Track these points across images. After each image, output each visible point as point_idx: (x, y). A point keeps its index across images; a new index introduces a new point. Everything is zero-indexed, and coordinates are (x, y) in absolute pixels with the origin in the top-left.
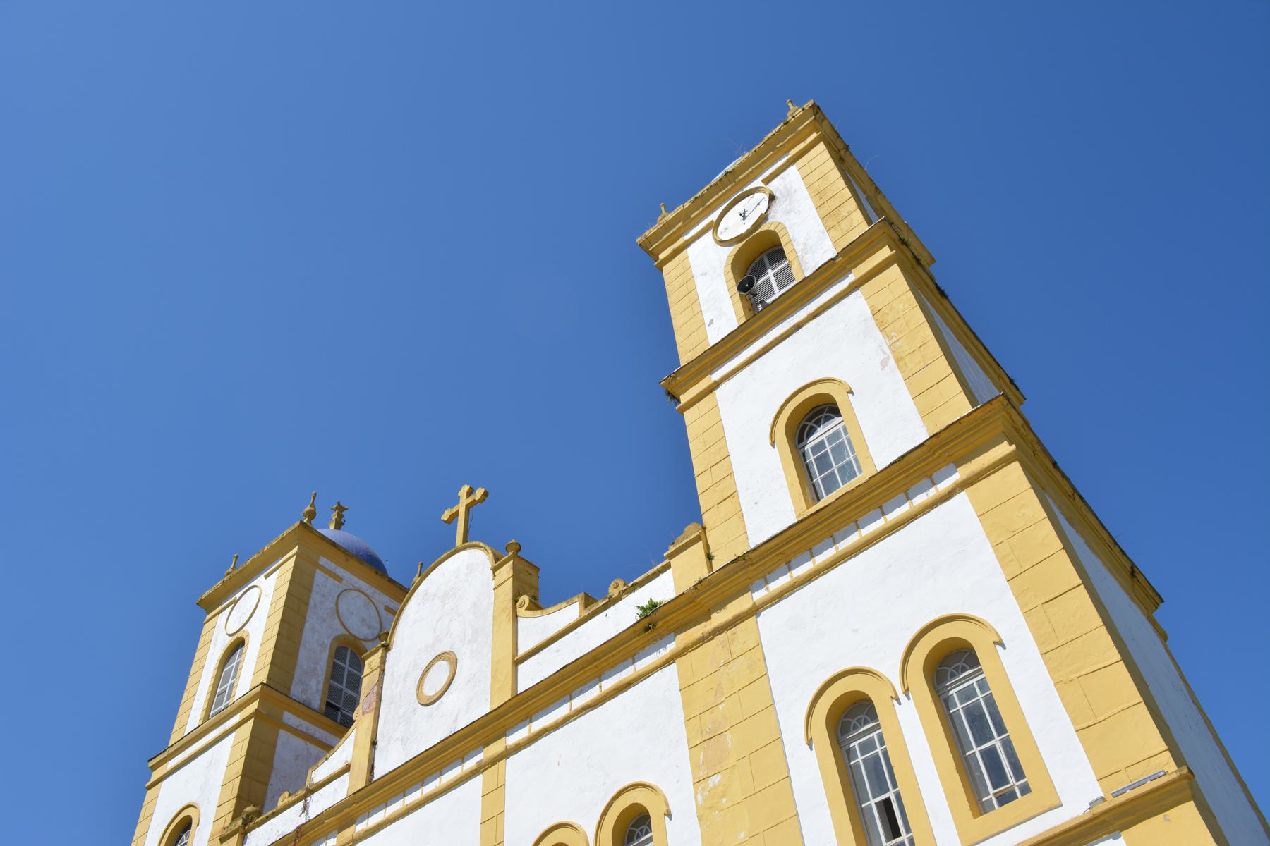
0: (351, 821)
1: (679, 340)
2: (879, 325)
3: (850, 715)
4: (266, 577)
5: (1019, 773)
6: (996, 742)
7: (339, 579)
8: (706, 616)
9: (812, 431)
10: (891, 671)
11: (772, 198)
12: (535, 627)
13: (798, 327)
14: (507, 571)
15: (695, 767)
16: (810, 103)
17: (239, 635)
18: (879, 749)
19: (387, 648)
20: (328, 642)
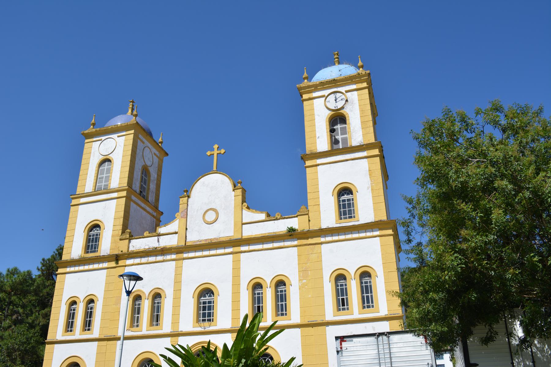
0: (182, 252)
1: (307, 137)
2: (370, 175)
4: (118, 137)
5: (372, 302)
6: (370, 295)
7: (143, 143)
8: (307, 238)
9: (343, 195)
11: (347, 101)
12: (249, 215)
13: (347, 160)
14: (239, 192)
15: (299, 276)
16: (368, 72)
17: (108, 157)
19: (189, 197)
20: (141, 168)
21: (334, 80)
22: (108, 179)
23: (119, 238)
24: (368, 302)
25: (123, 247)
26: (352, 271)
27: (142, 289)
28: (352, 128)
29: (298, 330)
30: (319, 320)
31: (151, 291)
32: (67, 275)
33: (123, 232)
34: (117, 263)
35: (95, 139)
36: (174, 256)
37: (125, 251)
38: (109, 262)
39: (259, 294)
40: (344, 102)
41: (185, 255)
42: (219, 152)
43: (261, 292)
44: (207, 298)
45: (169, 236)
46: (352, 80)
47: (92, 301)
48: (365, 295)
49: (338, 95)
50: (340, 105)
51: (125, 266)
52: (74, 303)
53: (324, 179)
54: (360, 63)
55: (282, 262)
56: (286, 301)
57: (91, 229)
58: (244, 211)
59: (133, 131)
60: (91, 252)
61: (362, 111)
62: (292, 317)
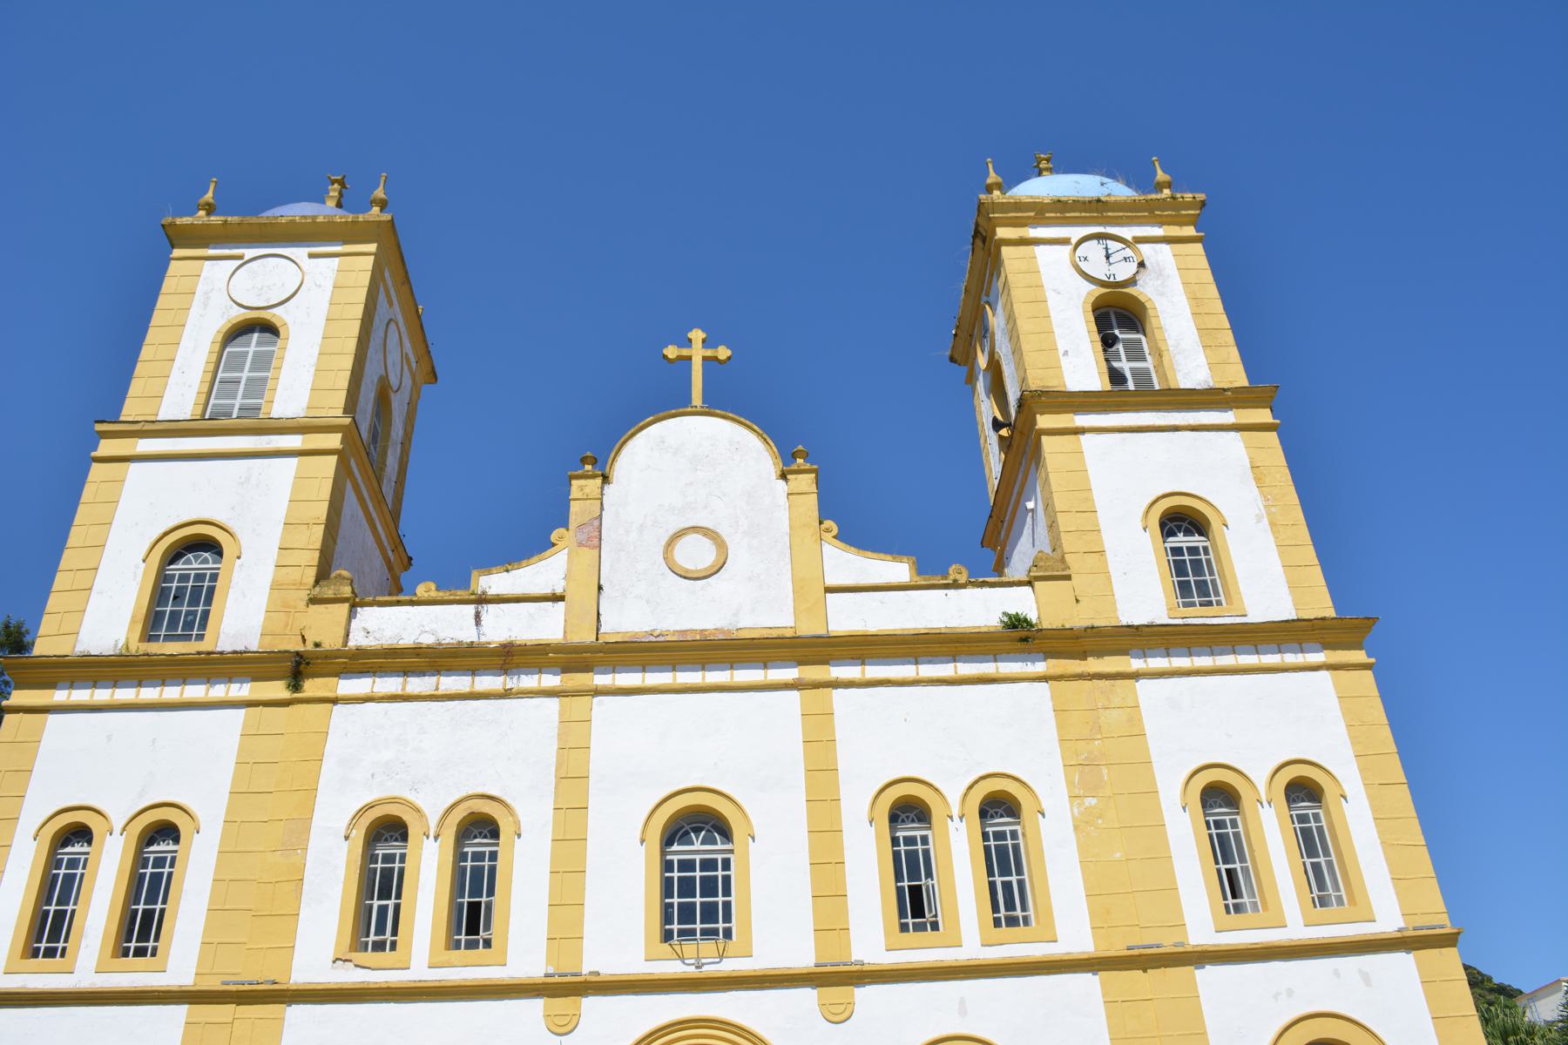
0: (587, 668)
2: (1257, 480)
3: (388, 830)
4: (311, 256)
8: (1083, 656)
10: (118, 822)
11: (1142, 265)
13: (1176, 429)
14: (806, 482)
15: (1070, 783)
18: (397, 865)
19: (606, 479)
21: (1099, 201)
22: (258, 387)
23: (304, 595)
24: (1010, 905)
25: (325, 627)
26: (1259, 773)
27: (411, 797)
28: (1170, 342)
29: (1089, 983)
30: (1168, 944)
31: (370, 807)
32: (52, 718)
33: (323, 575)
34: (296, 686)
35: (212, 252)
36: (551, 681)
37: (331, 642)
38: (255, 679)
39: (389, 858)
40: (1133, 267)
41: (601, 680)
42: (709, 353)
43: (918, 833)
44: (697, 846)
45: (524, 602)
46: (1151, 211)
47: (81, 833)
48: (999, 880)
49: (1114, 246)
50: (1123, 272)
51: (335, 701)
52: (166, 831)
53: (1112, 477)
54: (1161, 176)
55: (997, 728)
56: (399, 896)
57: (176, 554)
58: (826, 548)
59: (372, 247)
60: (168, 638)
61: (1195, 300)
62: (171, 965)
